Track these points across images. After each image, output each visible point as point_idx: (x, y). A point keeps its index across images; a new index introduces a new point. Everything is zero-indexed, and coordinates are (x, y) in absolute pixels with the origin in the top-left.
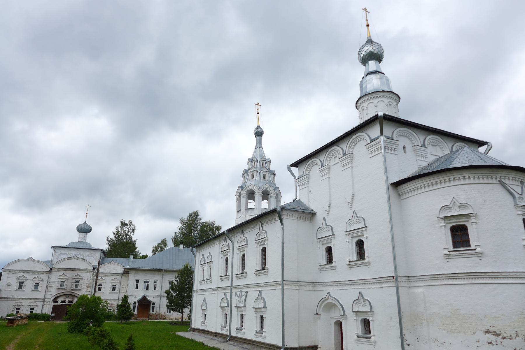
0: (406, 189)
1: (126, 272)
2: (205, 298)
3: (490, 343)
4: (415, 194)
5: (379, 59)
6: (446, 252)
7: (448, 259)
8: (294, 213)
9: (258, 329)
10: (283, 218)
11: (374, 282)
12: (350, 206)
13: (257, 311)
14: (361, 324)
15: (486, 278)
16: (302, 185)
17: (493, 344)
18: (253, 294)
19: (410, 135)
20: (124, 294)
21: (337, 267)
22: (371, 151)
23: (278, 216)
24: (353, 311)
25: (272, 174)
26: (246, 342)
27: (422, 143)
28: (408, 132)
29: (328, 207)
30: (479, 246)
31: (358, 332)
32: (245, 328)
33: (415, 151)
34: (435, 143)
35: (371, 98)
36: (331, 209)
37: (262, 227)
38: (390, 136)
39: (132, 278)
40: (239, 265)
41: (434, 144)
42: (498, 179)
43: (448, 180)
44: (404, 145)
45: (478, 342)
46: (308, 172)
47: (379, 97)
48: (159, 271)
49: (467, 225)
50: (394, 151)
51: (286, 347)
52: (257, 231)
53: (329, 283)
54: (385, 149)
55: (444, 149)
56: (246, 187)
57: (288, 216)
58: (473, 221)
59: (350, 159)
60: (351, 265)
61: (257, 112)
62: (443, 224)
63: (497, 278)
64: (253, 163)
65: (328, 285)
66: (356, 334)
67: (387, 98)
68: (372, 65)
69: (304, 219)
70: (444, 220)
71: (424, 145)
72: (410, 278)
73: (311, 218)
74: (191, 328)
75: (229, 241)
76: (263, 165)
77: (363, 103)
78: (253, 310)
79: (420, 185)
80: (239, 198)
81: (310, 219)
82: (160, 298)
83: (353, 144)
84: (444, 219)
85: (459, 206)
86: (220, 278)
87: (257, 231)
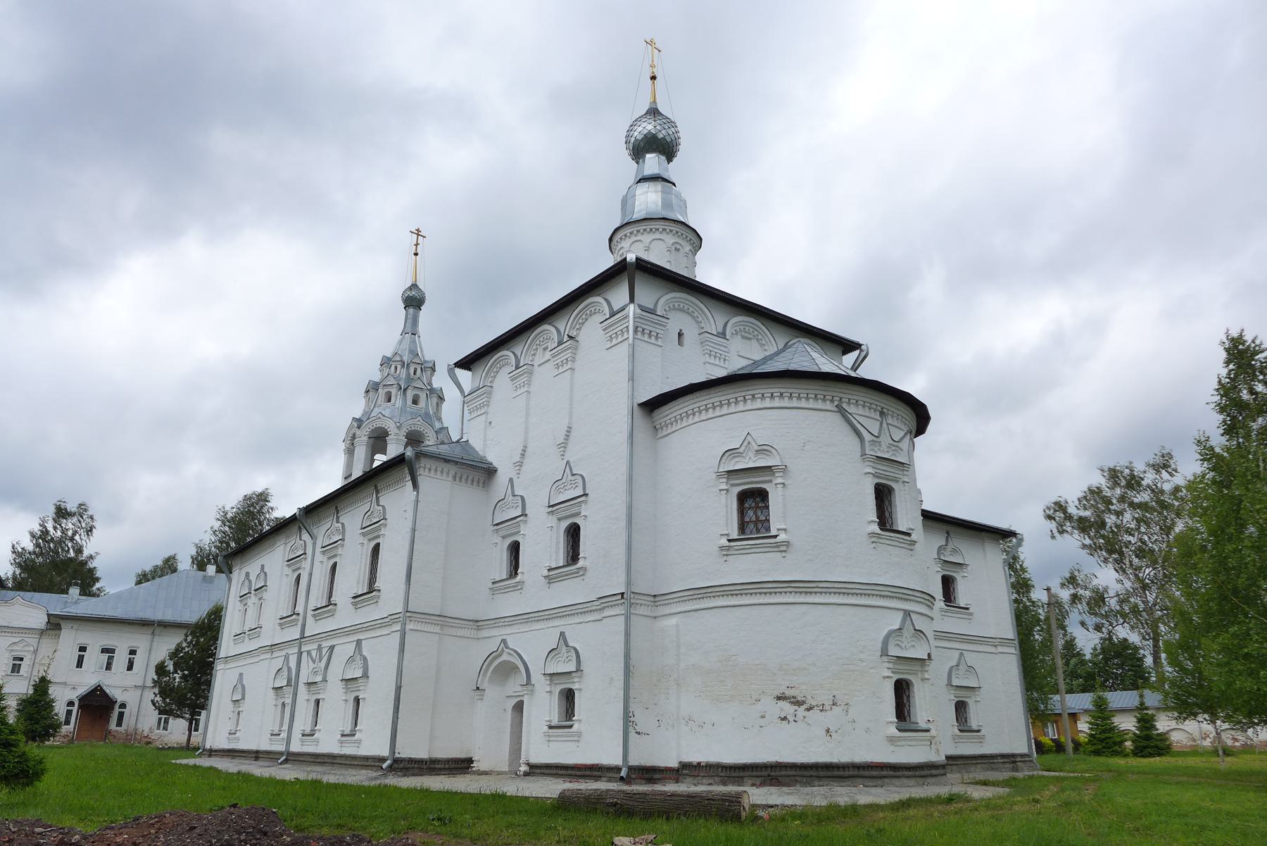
0: (668, 415)
1: (55, 624)
2: (241, 675)
3: (785, 719)
4: (682, 426)
5: (667, 151)
6: (724, 542)
7: (727, 555)
8: (446, 467)
9: (347, 727)
10: (420, 475)
11: (589, 609)
12: (562, 453)
13: (349, 686)
14: (558, 705)
15: (791, 592)
16: (478, 406)
17: (789, 721)
18: (345, 649)
19: (695, 309)
20: (42, 673)
21: (525, 584)
22: (611, 336)
23: (407, 471)
24: (544, 674)
25: (435, 395)
26: (320, 760)
27: (720, 330)
28: (692, 303)
29: (520, 456)
30: (785, 530)
31: (552, 718)
32: (320, 730)
33: (704, 344)
34: (750, 333)
35: (638, 231)
36: (526, 461)
37: (378, 498)
38: (652, 307)
39: (70, 638)
40: (321, 590)
41: (747, 335)
42: (836, 403)
43: (742, 398)
44: (681, 330)
45: (763, 717)
46: (490, 380)
47: (654, 230)
48: (144, 625)
49: (768, 490)
50: (657, 338)
51: (398, 758)
52: (367, 507)
53: (507, 620)
54: (636, 331)
55: (766, 348)
56: (371, 420)
57: (432, 471)
58: (780, 480)
59: (571, 352)
60: (553, 576)
61: (414, 251)
62: (724, 486)
63: (811, 593)
64: (393, 367)
65: (506, 623)
66: (547, 721)
67: (671, 234)
68: (653, 162)
69: (469, 481)
70: (728, 478)
71: (722, 335)
72: (657, 599)
73: (486, 482)
74: (204, 750)
75: (305, 536)
76: (414, 374)
77: (623, 242)
78: (341, 685)
79: (691, 407)
80: (352, 447)
81: (484, 483)
82: (140, 693)
83: (580, 321)
84: (726, 476)
85: (757, 451)
86: (279, 621)
87: (367, 507)
